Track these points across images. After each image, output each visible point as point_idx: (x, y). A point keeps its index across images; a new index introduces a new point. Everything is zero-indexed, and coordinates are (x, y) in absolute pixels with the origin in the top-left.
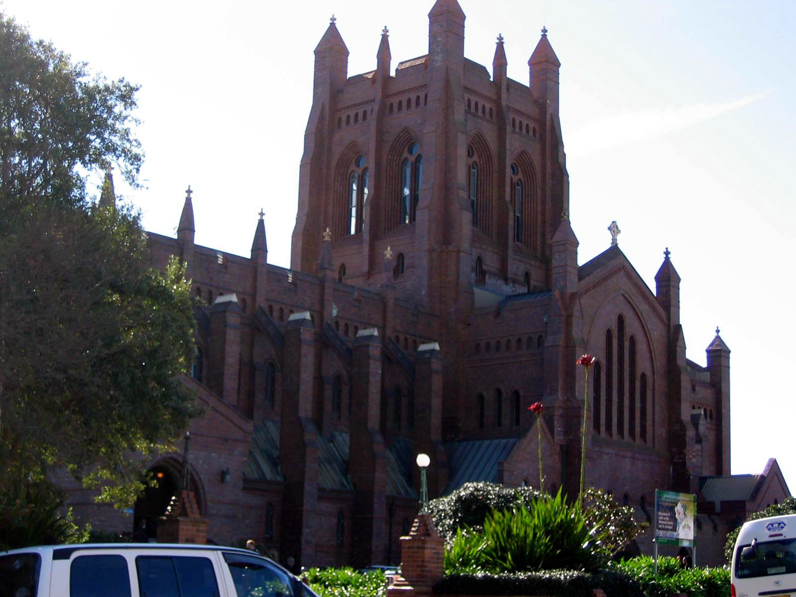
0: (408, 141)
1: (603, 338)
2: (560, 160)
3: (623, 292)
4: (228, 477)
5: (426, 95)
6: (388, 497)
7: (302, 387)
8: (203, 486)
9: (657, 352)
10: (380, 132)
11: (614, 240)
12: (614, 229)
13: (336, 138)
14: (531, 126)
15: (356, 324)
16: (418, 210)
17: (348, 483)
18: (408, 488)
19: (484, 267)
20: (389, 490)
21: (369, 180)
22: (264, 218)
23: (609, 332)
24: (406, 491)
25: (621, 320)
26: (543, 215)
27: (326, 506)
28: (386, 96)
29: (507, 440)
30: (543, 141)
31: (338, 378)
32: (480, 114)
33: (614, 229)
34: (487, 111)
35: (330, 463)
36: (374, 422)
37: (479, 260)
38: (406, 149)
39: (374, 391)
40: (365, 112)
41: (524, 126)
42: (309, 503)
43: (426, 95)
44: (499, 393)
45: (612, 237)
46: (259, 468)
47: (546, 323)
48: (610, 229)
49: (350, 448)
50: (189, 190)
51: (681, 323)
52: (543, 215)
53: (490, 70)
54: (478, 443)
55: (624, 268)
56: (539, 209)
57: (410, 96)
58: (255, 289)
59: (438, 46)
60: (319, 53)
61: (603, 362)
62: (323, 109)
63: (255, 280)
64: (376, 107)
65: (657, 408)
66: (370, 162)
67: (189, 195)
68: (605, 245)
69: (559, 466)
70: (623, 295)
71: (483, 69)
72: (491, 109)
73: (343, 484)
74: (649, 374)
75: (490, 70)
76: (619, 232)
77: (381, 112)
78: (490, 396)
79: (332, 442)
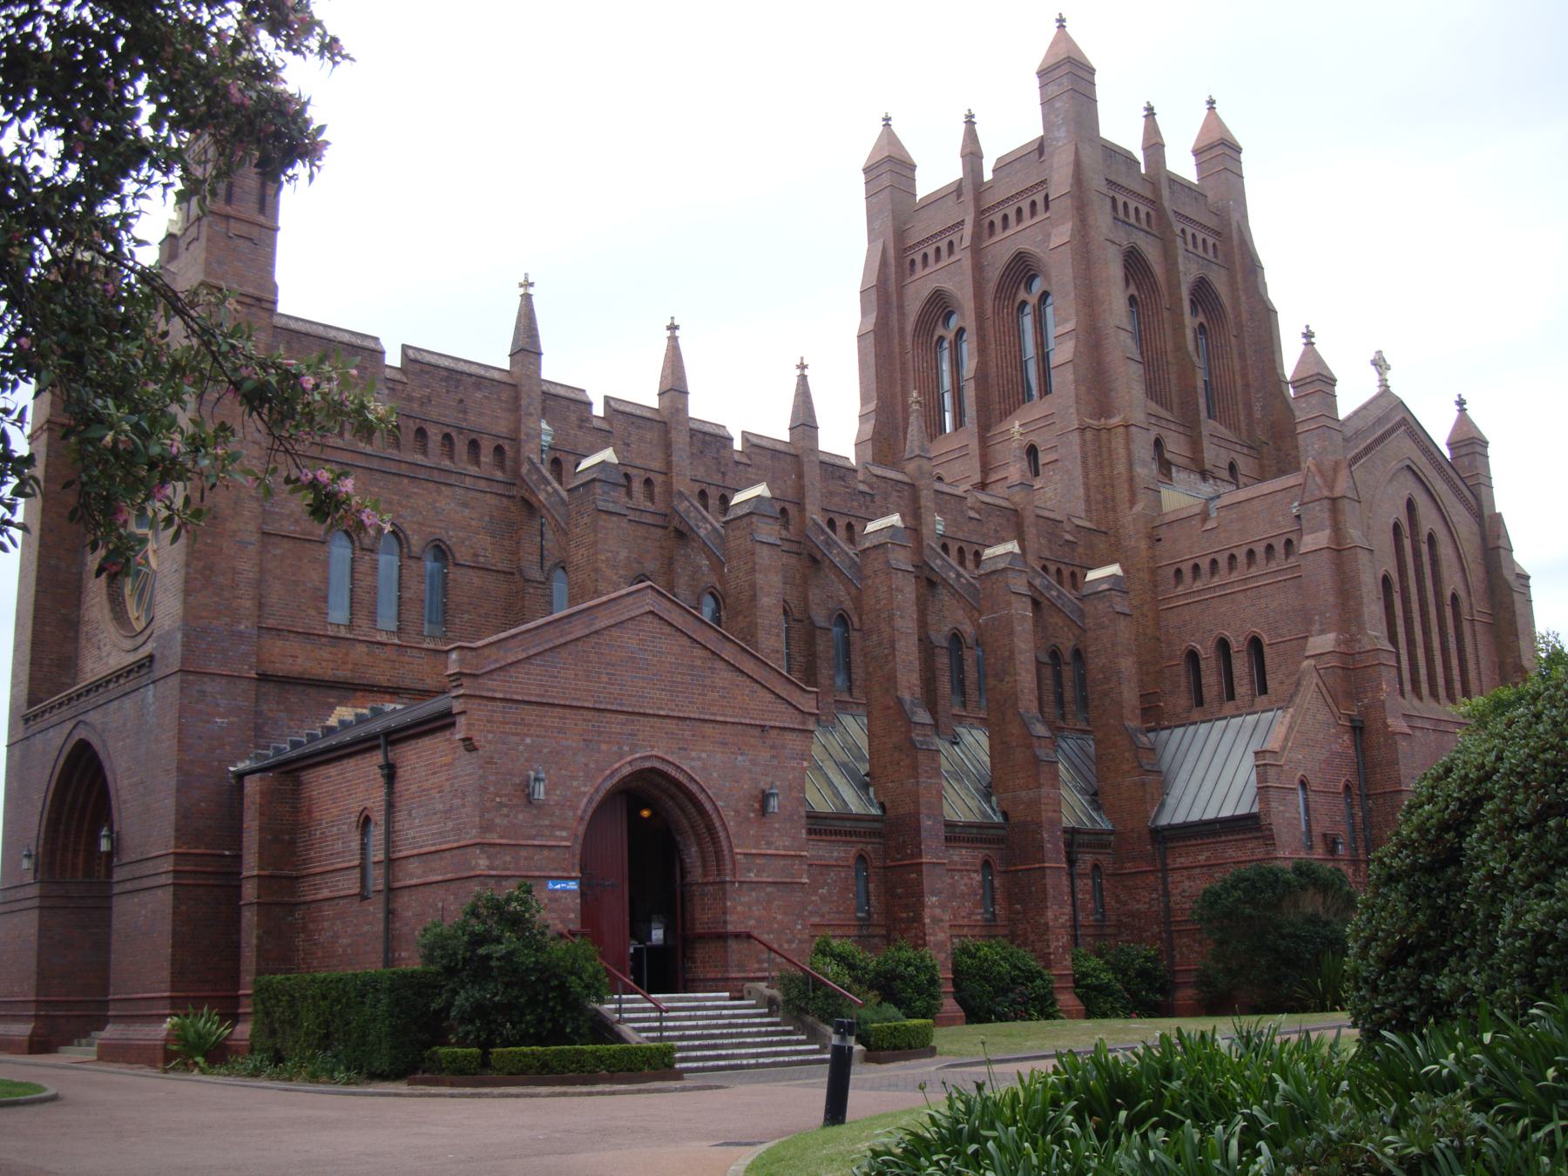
0: (1023, 269)
1: (1389, 537)
2: (1261, 289)
3: (1408, 462)
4: (774, 803)
5: (1047, 197)
6: (1066, 831)
7: (901, 645)
8: (723, 824)
9: (1470, 560)
10: (978, 268)
11: (1384, 384)
12: (1380, 364)
13: (910, 290)
14: (1210, 241)
15: (976, 547)
16: (855, 1088)
17: (995, 813)
18: (1094, 815)
19: (1168, 456)
20: (1068, 821)
21: (968, 349)
22: (806, 372)
23: (1396, 528)
24: (1091, 818)
25: (1411, 505)
26: (1244, 375)
27: (961, 855)
28: (980, 213)
29: (1255, 717)
30: (1230, 271)
31: (956, 638)
32: (1132, 220)
33: (1380, 364)
34: (1143, 216)
35: (959, 780)
36: (1028, 702)
37: (1158, 443)
38: (1022, 286)
39: (1023, 646)
40: (951, 244)
41: (1199, 242)
42: (932, 851)
43: (1047, 197)
44: (1223, 645)
45: (1377, 375)
46: (837, 794)
47: (1298, 517)
48: (1374, 363)
49: (991, 757)
50: (672, 324)
51: (1498, 510)
52: (1244, 375)
53: (1139, 156)
54: (1204, 728)
55: (1403, 422)
56: (1237, 368)
57: (1020, 204)
58: (801, 489)
59: (1057, 116)
60: (871, 171)
61: (1395, 576)
62: (884, 250)
63: (800, 476)
64: (968, 230)
65: (1481, 654)
66: (965, 317)
67: (673, 333)
68: (1371, 389)
69: (1351, 752)
70: (1408, 467)
71: (1128, 158)
72: (1148, 214)
73: (984, 813)
74: (1462, 594)
75: (1139, 156)
76: (1388, 368)
77: (977, 237)
78: (1207, 651)
79: (957, 744)
